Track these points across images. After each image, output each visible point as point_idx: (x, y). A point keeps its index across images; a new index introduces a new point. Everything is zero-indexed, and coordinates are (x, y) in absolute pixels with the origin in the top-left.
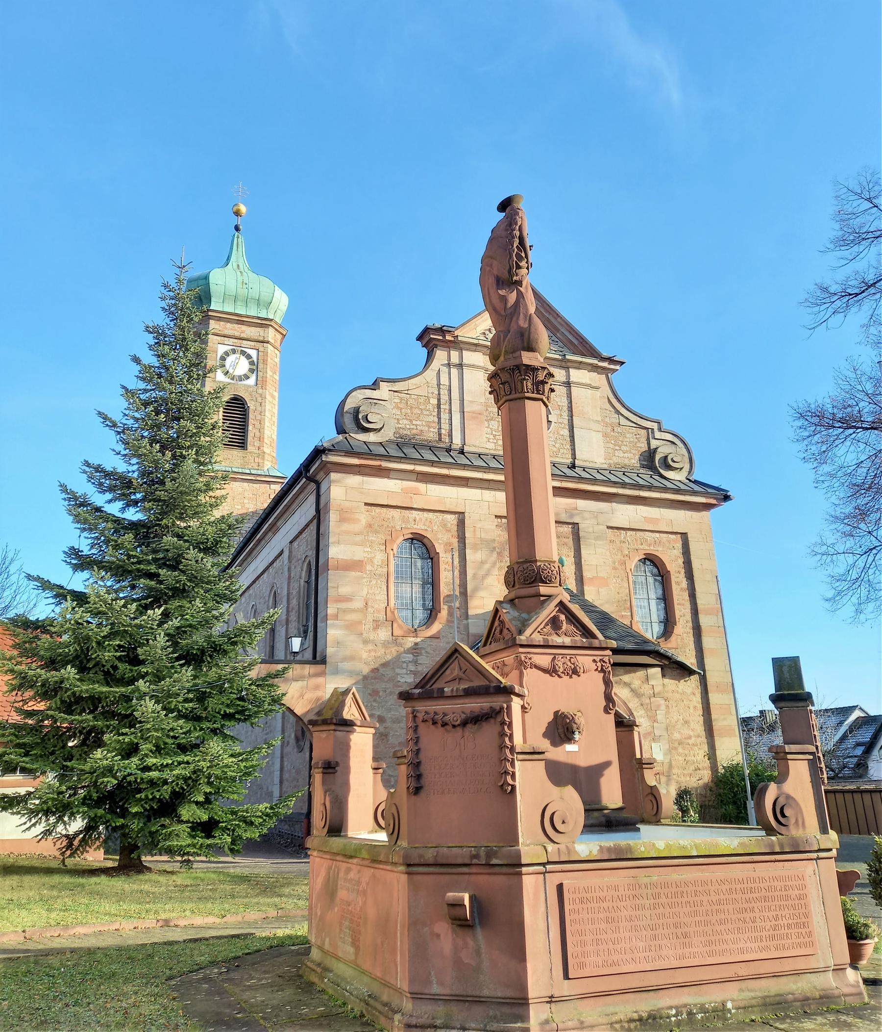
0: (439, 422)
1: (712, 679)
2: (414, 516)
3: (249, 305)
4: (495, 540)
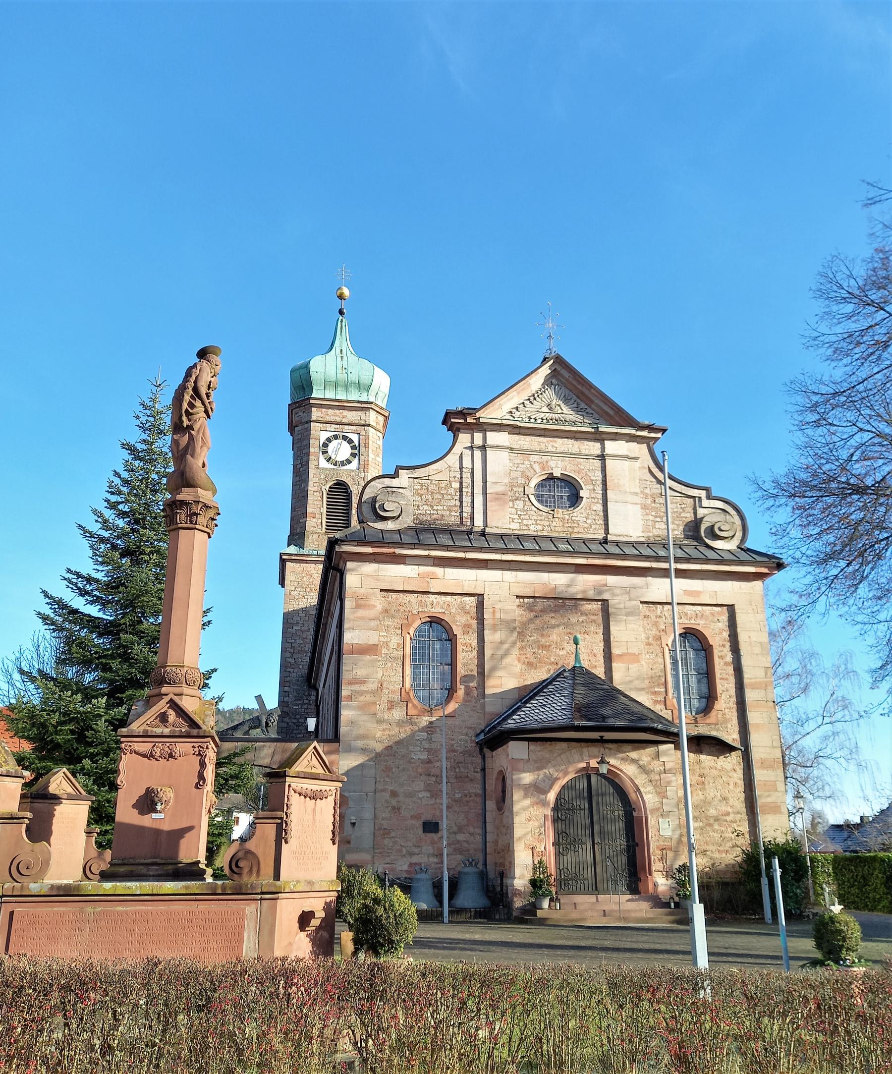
0: (461, 506)
1: (757, 753)
2: (431, 599)
3: (350, 389)
4: (515, 620)
